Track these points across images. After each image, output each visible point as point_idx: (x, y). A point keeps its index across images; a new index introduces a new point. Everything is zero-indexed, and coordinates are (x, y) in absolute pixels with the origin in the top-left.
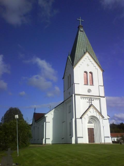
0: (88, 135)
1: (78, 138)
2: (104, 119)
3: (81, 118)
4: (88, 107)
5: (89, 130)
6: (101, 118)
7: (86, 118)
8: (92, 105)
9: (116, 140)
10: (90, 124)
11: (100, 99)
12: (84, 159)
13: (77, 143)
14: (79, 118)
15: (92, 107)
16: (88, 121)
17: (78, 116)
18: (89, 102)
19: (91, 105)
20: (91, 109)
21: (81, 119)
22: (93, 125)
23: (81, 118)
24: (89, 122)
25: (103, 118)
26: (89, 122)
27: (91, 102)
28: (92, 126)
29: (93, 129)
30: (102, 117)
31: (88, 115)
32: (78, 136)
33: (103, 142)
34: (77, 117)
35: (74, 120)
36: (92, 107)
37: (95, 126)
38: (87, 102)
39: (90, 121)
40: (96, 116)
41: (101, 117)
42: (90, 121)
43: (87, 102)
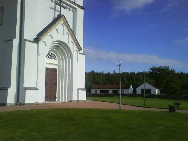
0: (46, 84)
1: (27, 91)
2: (80, 53)
3: (37, 40)
4: (51, 21)
5: (47, 72)
6: (77, 49)
7: (48, 41)
8: (63, 18)
9: (99, 92)
10: (51, 59)
11: (75, 9)
12: (155, 71)
13: (21, 101)
14: (32, 40)
15: (61, 22)
16: (48, 53)
17: (30, 34)
18: (55, 9)
19: (60, 16)
20: (59, 26)
21: (37, 45)
22: (56, 62)
23: (37, 40)
24: (50, 56)
25: (79, 50)
26: (50, 56)
27: (60, 11)
28: (53, 64)
29: (55, 70)
30: (78, 48)
31: (52, 39)
32: (25, 86)
33: (75, 99)
34: (26, 36)
35: (16, 42)
36: (62, 22)
37: (59, 66)
38: (51, 8)
39: (52, 52)
40: (67, 43)
41: (76, 48)
42: (52, 52)
43: (51, 8)
